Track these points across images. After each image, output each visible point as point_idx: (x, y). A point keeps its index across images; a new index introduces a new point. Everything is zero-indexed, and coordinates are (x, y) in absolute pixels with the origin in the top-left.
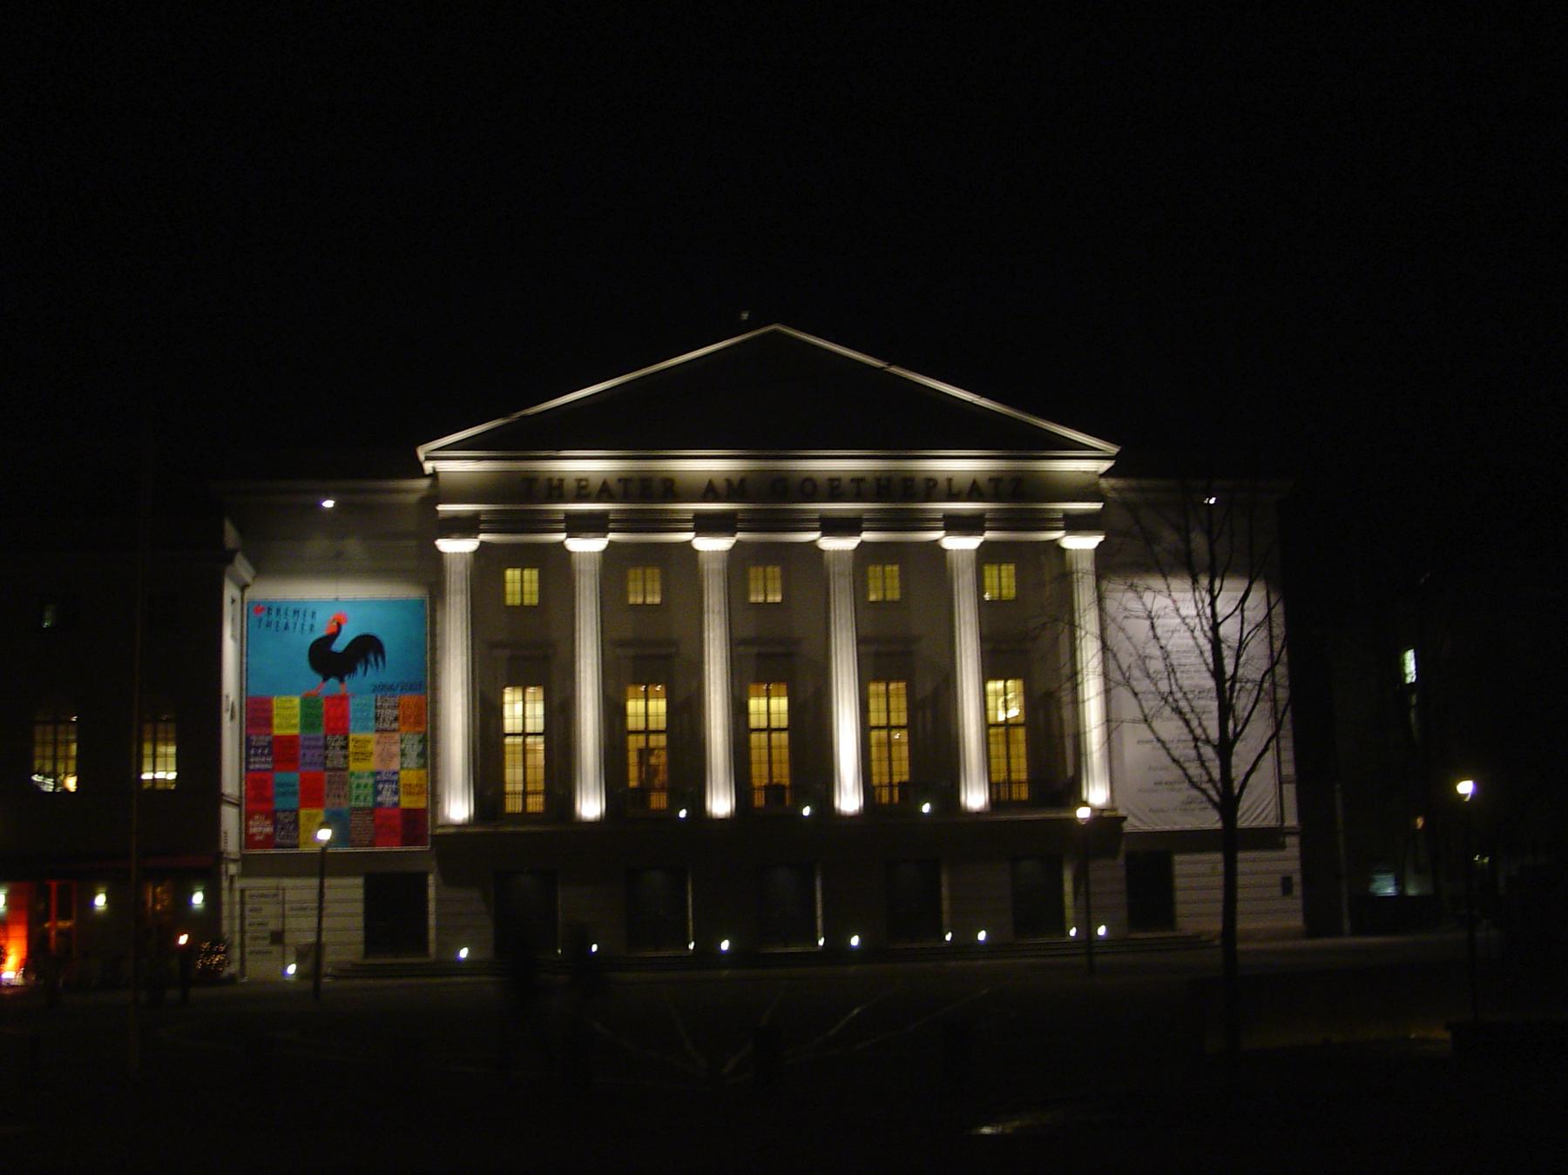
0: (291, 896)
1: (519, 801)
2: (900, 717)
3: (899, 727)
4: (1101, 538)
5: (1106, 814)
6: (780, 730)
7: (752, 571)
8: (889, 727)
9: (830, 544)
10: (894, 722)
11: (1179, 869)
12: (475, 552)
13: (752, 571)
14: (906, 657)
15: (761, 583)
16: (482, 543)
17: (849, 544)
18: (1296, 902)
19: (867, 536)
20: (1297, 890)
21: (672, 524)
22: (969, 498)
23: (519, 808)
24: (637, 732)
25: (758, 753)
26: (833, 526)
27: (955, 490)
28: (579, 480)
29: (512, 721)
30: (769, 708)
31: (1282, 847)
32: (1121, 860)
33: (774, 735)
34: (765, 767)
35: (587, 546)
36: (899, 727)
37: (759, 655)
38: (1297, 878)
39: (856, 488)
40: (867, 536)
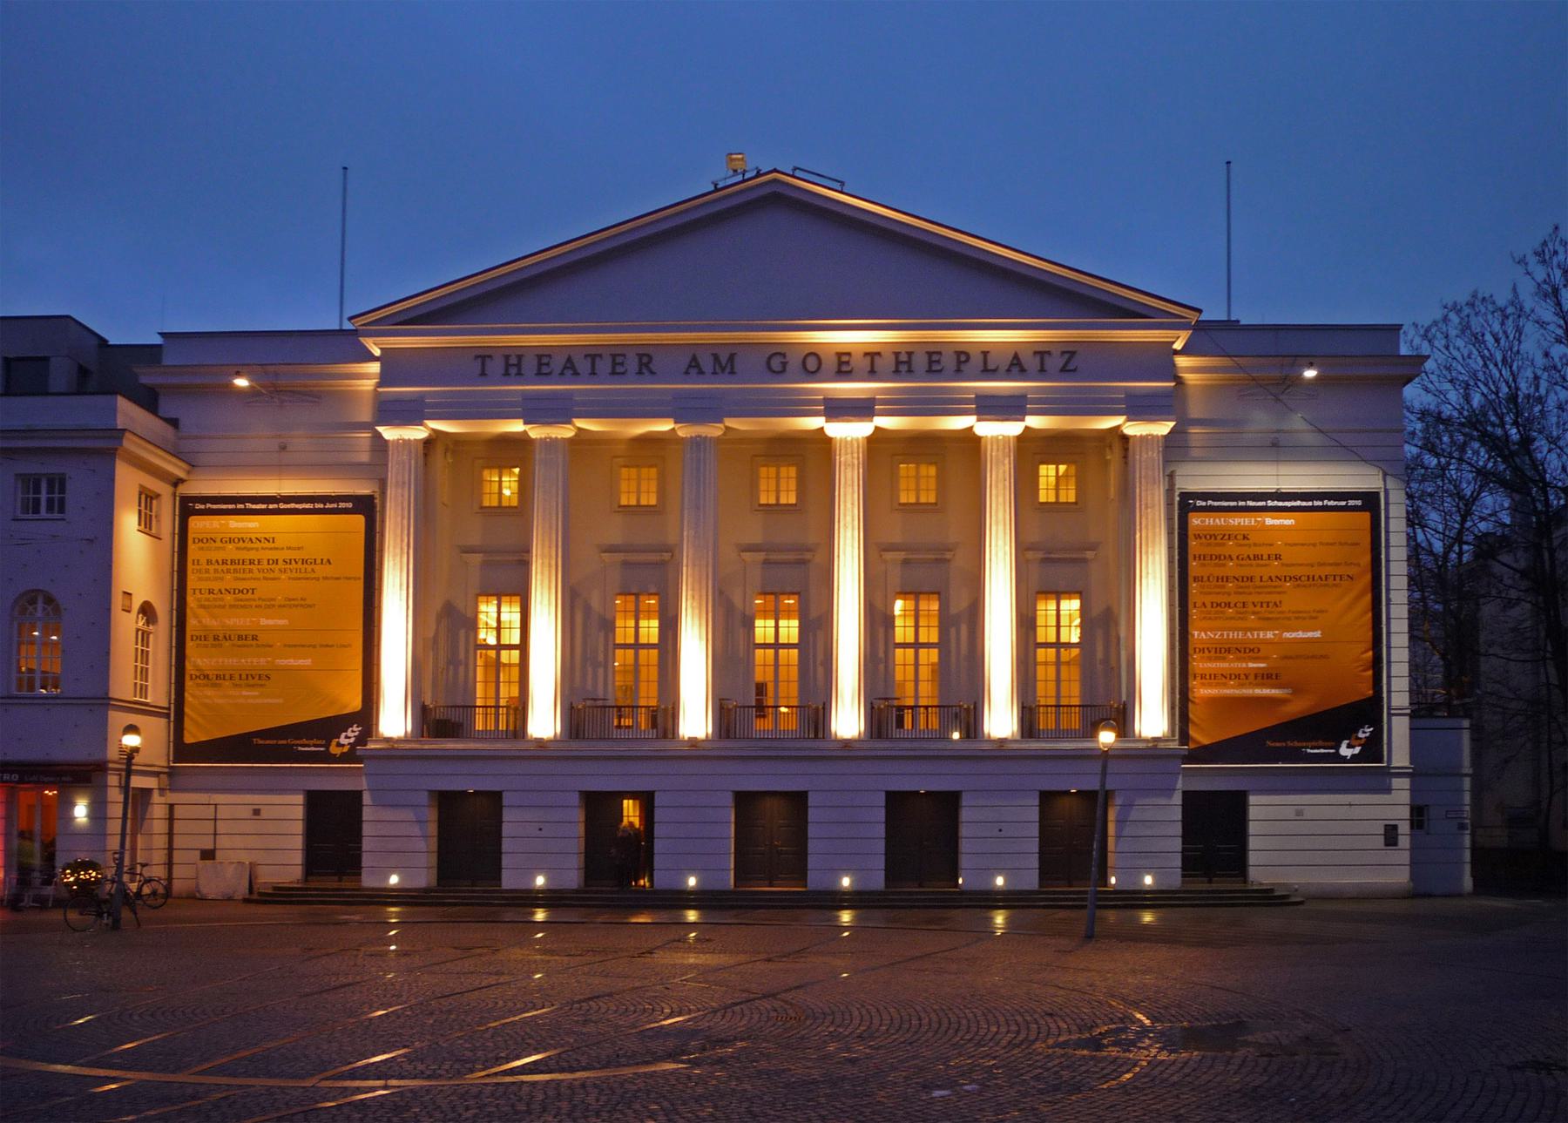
0: (223, 812)
1: (1052, 718)
2: (930, 634)
3: (928, 645)
4: (1172, 424)
5: (1161, 745)
6: (788, 646)
7: (763, 471)
8: (917, 645)
9: (988, 429)
10: (923, 639)
11: (1253, 812)
12: (1165, 437)
13: (763, 471)
14: (922, 564)
15: (773, 483)
16: (877, 428)
17: (1013, 429)
18: (1402, 855)
19: (1035, 422)
20: (1404, 841)
21: (802, 407)
22: (1008, 375)
23: (1052, 725)
24: (765, 646)
25: (1045, 674)
26: (990, 407)
27: (991, 366)
28: (839, 355)
29: (903, 631)
30: (1065, 618)
31: (1388, 790)
32: (1177, 799)
33: (643, 652)
34: (1052, 686)
35: (850, 432)
36: (928, 645)
37: (906, 562)
38: (1404, 828)
39: (872, 363)
40: (1035, 422)
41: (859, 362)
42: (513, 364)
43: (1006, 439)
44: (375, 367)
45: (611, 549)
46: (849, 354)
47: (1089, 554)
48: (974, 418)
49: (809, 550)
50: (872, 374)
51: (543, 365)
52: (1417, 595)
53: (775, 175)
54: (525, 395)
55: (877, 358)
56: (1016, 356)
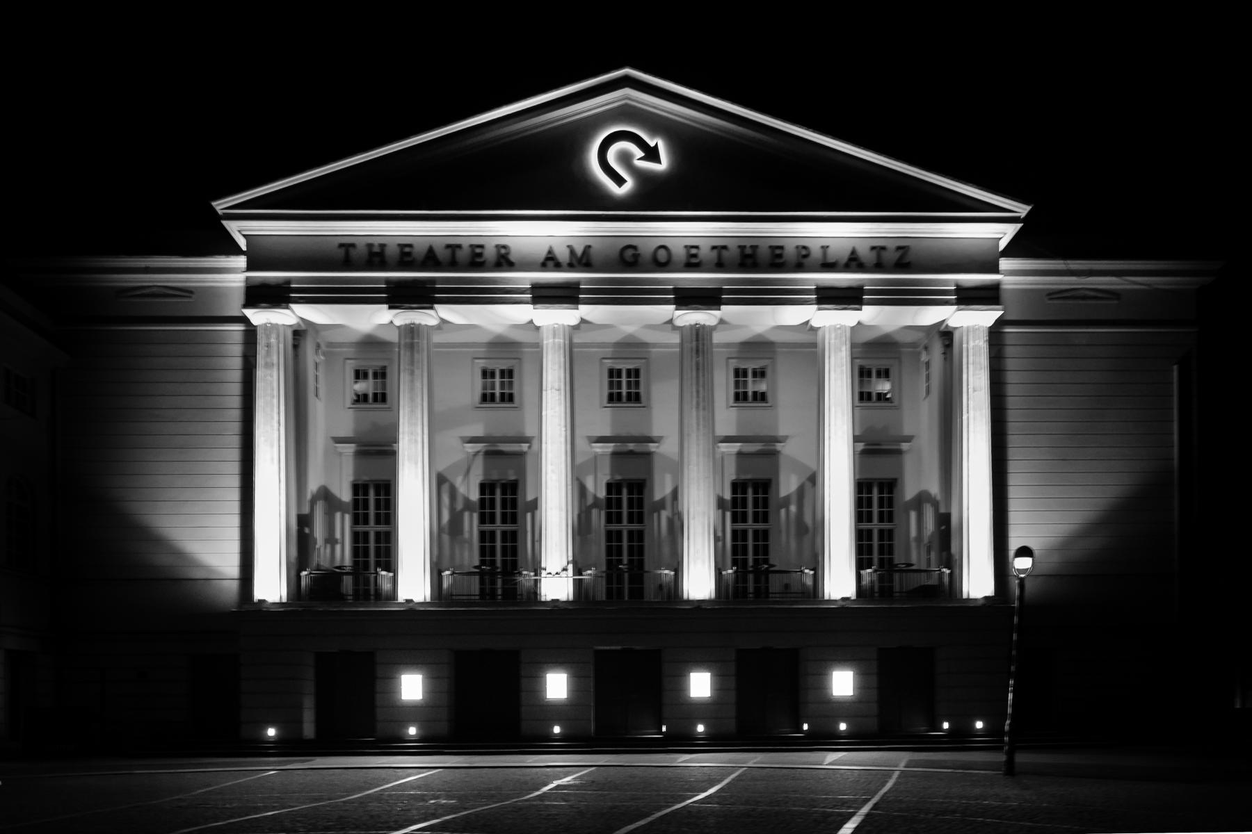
4: (1000, 313)
12: (852, 328)
16: (583, 321)
17: (846, 318)
26: (829, 297)
27: (831, 260)
41: (463, 255)
42: (376, 256)
43: (842, 328)
44: (241, 261)
45: (473, 440)
46: (410, 246)
47: (905, 446)
48: (673, 307)
49: (653, 442)
50: (720, 266)
51: (406, 256)
52: (307, 530)
53: (628, 91)
54: (388, 281)
55: (351, 250)
56: (550, 252)
